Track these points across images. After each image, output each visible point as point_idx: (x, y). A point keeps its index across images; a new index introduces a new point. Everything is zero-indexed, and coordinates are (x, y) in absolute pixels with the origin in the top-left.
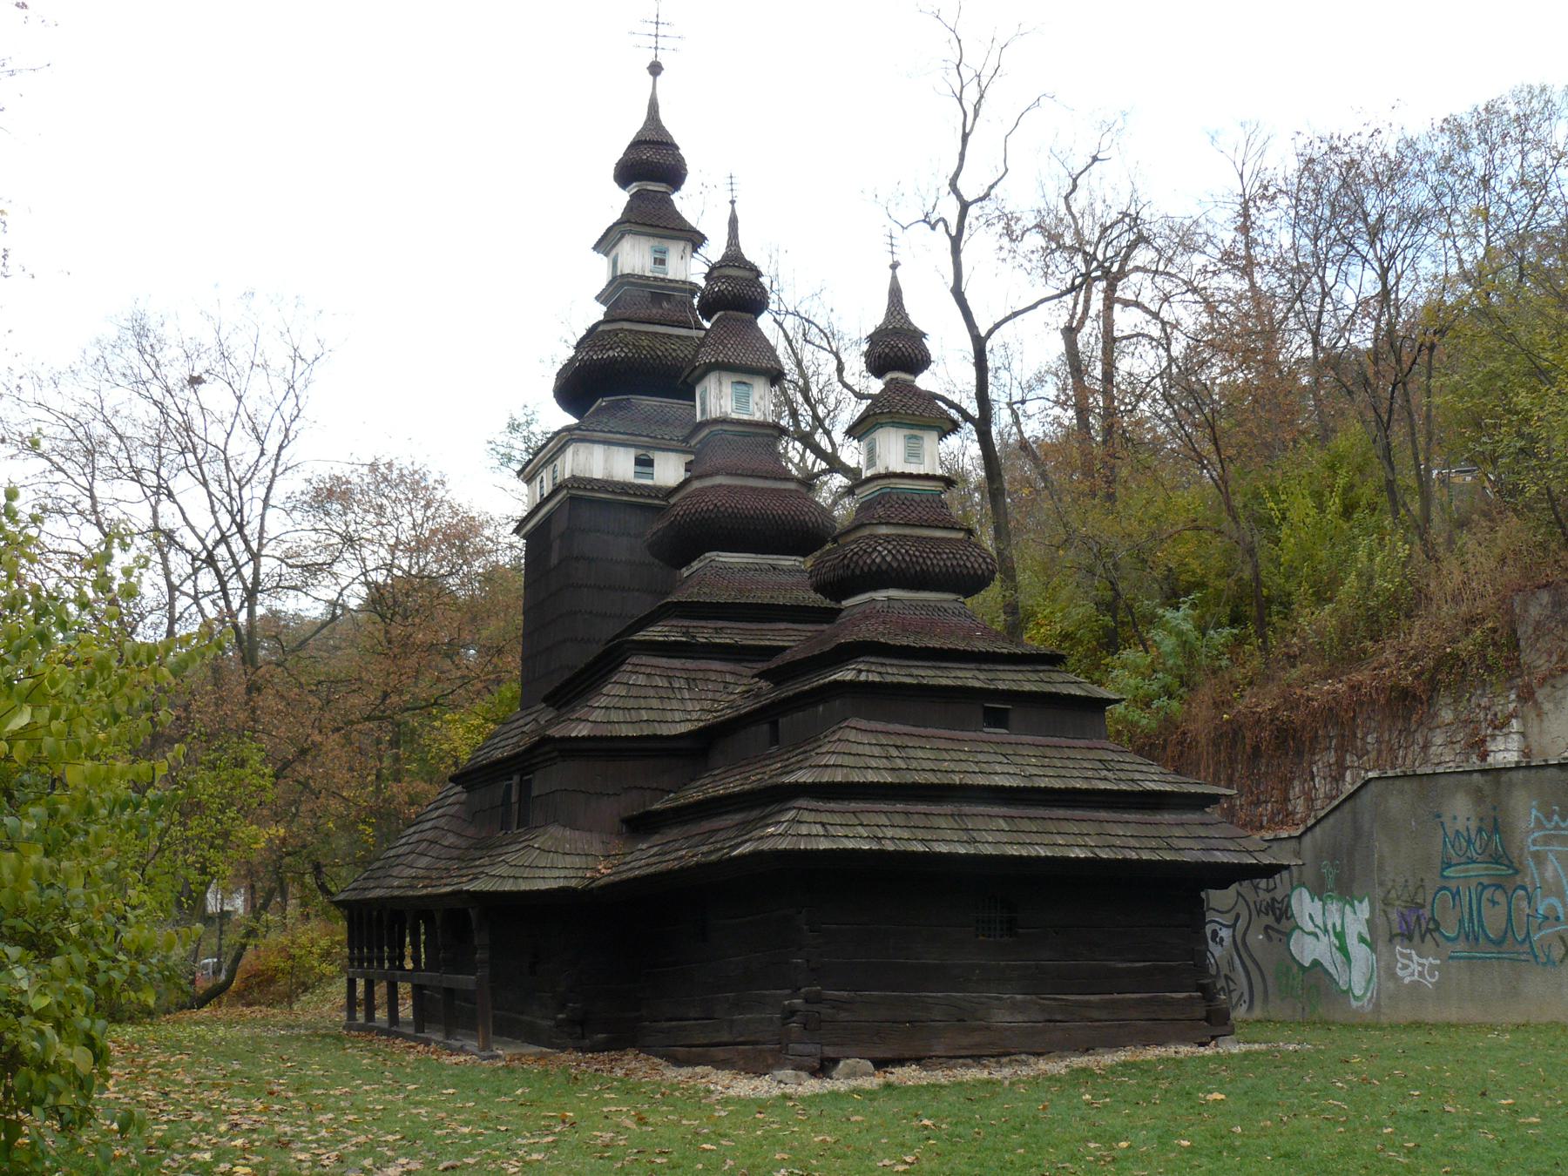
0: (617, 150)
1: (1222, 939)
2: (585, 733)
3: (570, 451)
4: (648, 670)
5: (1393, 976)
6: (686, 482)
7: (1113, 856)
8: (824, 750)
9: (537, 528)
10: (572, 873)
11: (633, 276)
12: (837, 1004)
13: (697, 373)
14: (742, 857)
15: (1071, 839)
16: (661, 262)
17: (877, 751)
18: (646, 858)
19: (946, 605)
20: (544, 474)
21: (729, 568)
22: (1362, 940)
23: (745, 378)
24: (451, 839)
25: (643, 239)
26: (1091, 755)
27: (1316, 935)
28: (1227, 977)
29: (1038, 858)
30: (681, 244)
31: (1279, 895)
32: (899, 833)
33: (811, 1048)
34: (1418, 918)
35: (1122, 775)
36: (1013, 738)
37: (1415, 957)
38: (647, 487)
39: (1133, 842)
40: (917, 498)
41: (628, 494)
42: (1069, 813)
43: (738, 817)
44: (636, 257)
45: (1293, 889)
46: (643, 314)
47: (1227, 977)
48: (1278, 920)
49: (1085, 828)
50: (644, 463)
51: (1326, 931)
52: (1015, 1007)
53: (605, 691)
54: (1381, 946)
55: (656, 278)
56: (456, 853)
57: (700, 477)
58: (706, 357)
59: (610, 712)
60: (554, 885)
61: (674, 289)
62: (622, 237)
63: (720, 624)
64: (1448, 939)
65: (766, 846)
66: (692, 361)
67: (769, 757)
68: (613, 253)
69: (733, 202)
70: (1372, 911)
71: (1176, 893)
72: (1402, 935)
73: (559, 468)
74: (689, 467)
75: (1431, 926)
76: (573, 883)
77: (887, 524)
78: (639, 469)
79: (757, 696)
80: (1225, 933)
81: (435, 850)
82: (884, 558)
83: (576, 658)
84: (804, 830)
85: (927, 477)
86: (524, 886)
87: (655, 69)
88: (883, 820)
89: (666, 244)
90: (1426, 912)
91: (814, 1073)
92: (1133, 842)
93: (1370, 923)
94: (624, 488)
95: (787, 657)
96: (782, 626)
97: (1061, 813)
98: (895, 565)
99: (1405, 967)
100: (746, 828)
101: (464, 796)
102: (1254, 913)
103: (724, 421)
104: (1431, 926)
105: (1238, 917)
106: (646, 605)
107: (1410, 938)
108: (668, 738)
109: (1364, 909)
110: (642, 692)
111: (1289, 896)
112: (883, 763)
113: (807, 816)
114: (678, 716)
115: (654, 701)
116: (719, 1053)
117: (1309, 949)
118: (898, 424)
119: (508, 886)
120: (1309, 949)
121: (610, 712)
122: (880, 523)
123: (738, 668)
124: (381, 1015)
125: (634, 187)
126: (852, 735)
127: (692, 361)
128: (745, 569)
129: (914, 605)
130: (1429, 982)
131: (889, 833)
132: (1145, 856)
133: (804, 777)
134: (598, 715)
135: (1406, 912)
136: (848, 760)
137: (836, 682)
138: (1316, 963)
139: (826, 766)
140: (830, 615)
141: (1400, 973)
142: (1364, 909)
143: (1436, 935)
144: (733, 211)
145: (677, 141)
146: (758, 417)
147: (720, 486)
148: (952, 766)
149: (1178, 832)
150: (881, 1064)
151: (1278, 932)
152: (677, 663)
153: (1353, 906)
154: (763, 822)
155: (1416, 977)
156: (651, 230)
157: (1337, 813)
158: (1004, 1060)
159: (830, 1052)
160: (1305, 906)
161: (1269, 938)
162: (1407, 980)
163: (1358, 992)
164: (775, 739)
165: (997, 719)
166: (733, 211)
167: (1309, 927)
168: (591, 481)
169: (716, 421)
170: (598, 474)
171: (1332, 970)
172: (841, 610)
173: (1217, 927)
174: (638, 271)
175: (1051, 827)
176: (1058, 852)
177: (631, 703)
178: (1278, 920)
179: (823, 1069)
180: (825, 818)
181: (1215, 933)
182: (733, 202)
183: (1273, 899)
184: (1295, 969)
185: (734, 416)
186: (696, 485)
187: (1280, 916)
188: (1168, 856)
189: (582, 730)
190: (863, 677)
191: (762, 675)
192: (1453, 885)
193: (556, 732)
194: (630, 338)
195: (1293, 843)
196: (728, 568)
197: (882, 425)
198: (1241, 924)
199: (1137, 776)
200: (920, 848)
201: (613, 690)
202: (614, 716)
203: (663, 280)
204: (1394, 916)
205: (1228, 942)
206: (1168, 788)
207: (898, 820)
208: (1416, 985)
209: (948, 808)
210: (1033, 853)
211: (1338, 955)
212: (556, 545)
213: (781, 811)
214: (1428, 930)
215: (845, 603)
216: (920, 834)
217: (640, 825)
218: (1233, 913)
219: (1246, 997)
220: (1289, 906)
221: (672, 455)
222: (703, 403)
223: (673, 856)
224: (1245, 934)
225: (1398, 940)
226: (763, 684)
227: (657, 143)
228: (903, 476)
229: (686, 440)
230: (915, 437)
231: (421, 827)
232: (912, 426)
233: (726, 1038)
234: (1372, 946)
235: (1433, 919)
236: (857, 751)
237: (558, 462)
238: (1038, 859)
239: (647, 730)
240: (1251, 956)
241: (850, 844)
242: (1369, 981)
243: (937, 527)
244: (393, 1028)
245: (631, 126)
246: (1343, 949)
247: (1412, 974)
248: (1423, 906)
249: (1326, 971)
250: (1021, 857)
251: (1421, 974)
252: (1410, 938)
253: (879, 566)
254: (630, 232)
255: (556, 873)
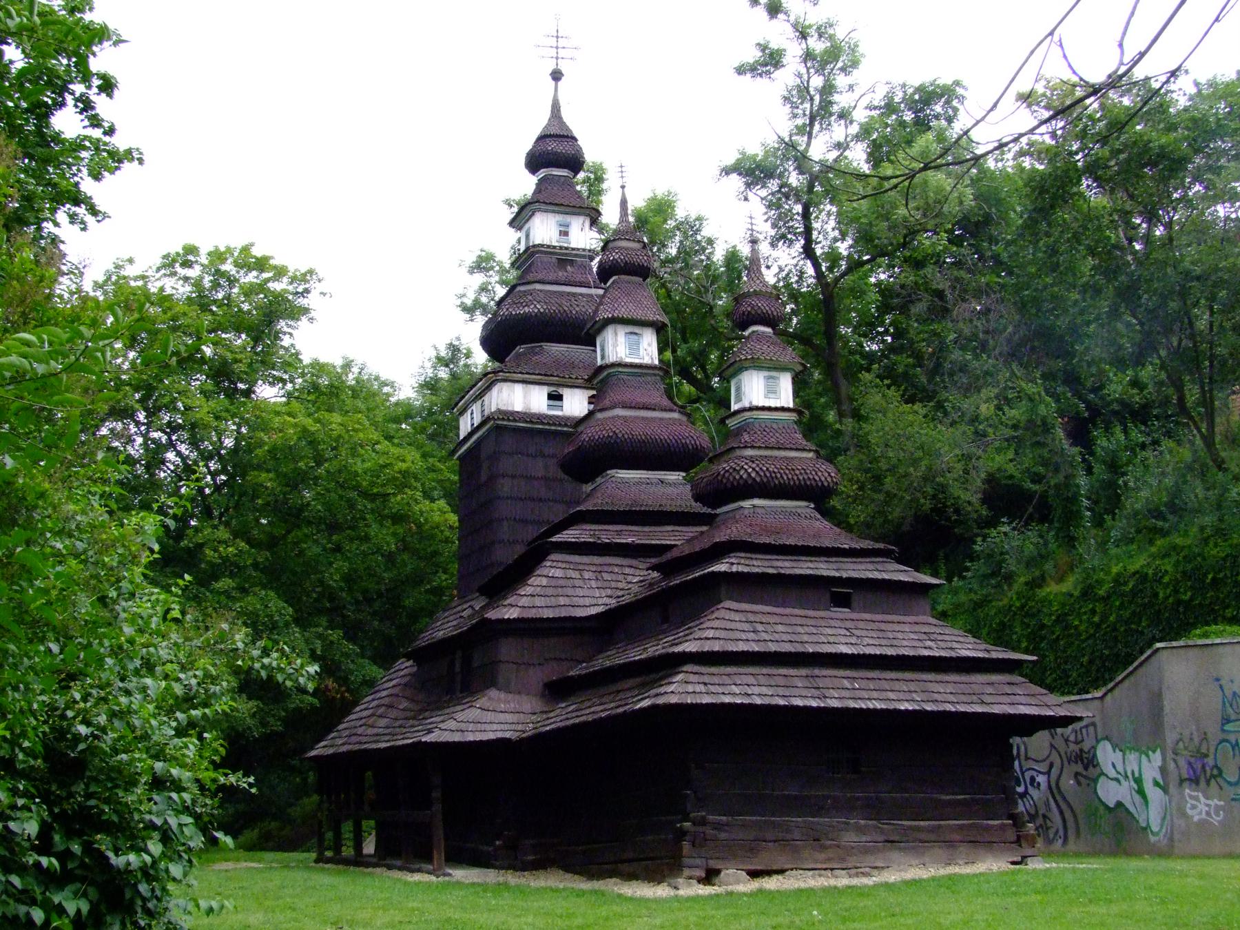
0: (527, 143)
1: (1039, 784)
2: (515, 616)
3: (495, 390)
4: (564, 565)
5: (1184, 814)
6: (591, 414)
7: (935, 708)
8: (704, 626)
9: (469, 450)
10: (506, 727)
11: (542, 246)
12: (718, 826)
13: (597, 326)
14: (641, 709)
15: (901, 696)
16: (565, 234)
17: (746, 627)
18: (565, 715)
19: (799, 511)
20: (474, 407)
21: (629, 483)
22: (1156, 784)
23: (636, 329)
24: (404, 704)
25: (550, 215)
26: (917, 628)
27: (1117, 780)
28: (1044, 816)
29: (875, 711)
30: (581, 219)
31: (1086, 746)
32: (764, 690)
33: (698, 861)
34: (1203, 767)
35: (942, 644)
36: (855, 616)
37: (1202, 799)
38: (558, 417)
39: (951, 698)
40: (775, 426)
41: (543, 423)
42: (899, 675)
43: (638, 680)
44: (544, 230)
45: (1098, 741)
46: (551, 277)
47: (1044, 816)
48: (1086, 768)
49: (912, 686)
50: (555, 397)
51: (1127, 777)
52: (860, 830)
53: (529, 582)
54: (1173, 789)
55: (561, 248)
56: (409, 714)
57: (601, 410)
58: (604, 314)
59: (532, 599)
60: (492, 736)
61: (576, 255)
62: (533, 214)
63: (619, 527)
64: (1229, 783)
65: (661, 701)
66: (593, 317)
67: (664, 632)
68: (526, 226)
69: (623, 187)
70: (1164, 759)
71: (991, 738)
72: (1190, 780)
73: (486, 403)
74: (591, 400)
75: (1215, 772)
76: (508, 735)
77: (753, 447)
78: (552, 402)
79: (651, 585)
80: (1041, 779)
81: (393, 713)
82: (749, 474)
83: (506, 555)
84: (690, 688)
85: (783, 409)
86: (471, 737)
87: (557, 76)
88: (751, 680)
89: (568, 218)
90: (1210, 761)
91: (700, 881)
92: (951, 698)
93: (1163, 770)
94: (540, 418)
95: (675, 553)
96: (669, 528)
97: (893, 675)
98: (758, 479)
99: (1194, 807)
100: (645, 686)
101: (415, 669)
102: (1066, 763)
103: (620, 365)
104: (1215, 772)
105: (1051, 765)
106: (558, 513)
107: (1197, 782)
108: (581, 618)
109: (1157, 758)
110: (561, 582)
111: (1094, 748)
112: (751, 636)
113: (692, 678)
114: (587, 601)
115: (571, 588)
116: (625, 867)
117: (1111, 792)
118: (760, 368)
119: (457, 737)
120: (1111, 792)
121: (532, 599)
122: (746, 447)
123: (634, 562)
124: (348, 851)
125: (542, 173)
126: (728, 615)
127: (593, 317)
128: (639, 483)
129: (774, 511)
130: (1216, 820)
131: (756, 690)
132: (961, 708)
133: (690, 647)
134: (524, 601)
135: (1192, 760)
136: (722, 634)
137: (713, 572)
138: (1119, 804)
139: (707, 639)
140: (708, 520)
141: (1189, 812)
142: (1157, 758)
143: (1219, 779)
144: (623, 194)
145: (576, 134)
146: (647, 361)
147: (618, 416)
148: (806, 638)
149: (990, 690)
150: (754, 874)
151: (1085, 777)
152: (585, 559)
153: (1148, 756)
154: (656, 683)
155: (1204, 816)
156: (556, 208)
157: (1132, 678)
158: (853, 871)
159: (713, 864)
160: (1106, 755)
161: (1079, 783)
162: (1196, 819)
163: (1155, 828)
164: (665, 620)
165: (842, 601)
166: (623, 194)
167: (1112, 774)
168: (513, 413)
169: (613, 365)
170: (518, 407)
171: (1132, 809)
172: (717, 515)
173: (1035, 774)
174: (547, 242)
175: (885, 685)
176: (891, 706)
177: (550, 591)
178: (1086, 768)
179: (710, 877)
180: (706, 679)
181: (1033, 779)
182: (623, 187)
183: (1081, 750)
184: (1102, 808)
185: (628, 360)
186: (599, 415)
187: (1086, 762)
188: (979, 709)
189: (512, 614)
190: (734, 569)
191: (653, 568)
192: (1232, 738)
193: (492, 615)
194: (542, 295)
195: (1097, 703)
196: (625, 482)
197: (747, 369)
198: (1055, 772)
199: (955, 645)
200: (782, 702)
201: (537, 582)
202: (538, 602)
203: (566, 248)
204: (1182, 763)
205: (1044, 786)
206: (981, 655)
207: (763, 680)
208: (1202, 823)
209: (803, 672)
210: (871, 706)
211: (1137, 797)
212: (485, 466)
213: (671, 675)
214: (1213, 776)
215: (719, 511)
216: (781, 691)
217: (557, 691)
218: (1047, 762)
219: (1061, 833)
220: (1095, 756)
221: (577, 391)
222: (603, 350)
223: (588, 711)
224: (1057, 784)
225: (1186, 784)
226: (655, 574)
227: (563, 136)
228: (763, 409)
229: (590, 380)
230: (772, 377)
231: (378, 695)
232: (769, 369)
233: (631, 855)
234: (1165, 790)
235: (1216, 766)
236: (730, 626)
237: (486, 398)
238: (875, 711)
239: (564, 613)
240: (1064, 798)
241: (727, 699)
242: (1164, 819)
243: (791, 449)
244: (359, 861)
245: (538, 123)
246: (1141, 792)
247: (1200, 813)
248: (1206, 756)
249: (1127, 809)
250: (861, 709)
251: (1208, 813)
252: (1197, 782)
253: (746, 481)
254: (540, 210)
255: (495, 727)
